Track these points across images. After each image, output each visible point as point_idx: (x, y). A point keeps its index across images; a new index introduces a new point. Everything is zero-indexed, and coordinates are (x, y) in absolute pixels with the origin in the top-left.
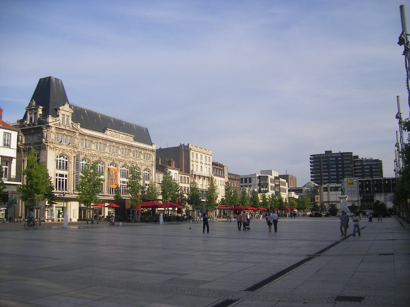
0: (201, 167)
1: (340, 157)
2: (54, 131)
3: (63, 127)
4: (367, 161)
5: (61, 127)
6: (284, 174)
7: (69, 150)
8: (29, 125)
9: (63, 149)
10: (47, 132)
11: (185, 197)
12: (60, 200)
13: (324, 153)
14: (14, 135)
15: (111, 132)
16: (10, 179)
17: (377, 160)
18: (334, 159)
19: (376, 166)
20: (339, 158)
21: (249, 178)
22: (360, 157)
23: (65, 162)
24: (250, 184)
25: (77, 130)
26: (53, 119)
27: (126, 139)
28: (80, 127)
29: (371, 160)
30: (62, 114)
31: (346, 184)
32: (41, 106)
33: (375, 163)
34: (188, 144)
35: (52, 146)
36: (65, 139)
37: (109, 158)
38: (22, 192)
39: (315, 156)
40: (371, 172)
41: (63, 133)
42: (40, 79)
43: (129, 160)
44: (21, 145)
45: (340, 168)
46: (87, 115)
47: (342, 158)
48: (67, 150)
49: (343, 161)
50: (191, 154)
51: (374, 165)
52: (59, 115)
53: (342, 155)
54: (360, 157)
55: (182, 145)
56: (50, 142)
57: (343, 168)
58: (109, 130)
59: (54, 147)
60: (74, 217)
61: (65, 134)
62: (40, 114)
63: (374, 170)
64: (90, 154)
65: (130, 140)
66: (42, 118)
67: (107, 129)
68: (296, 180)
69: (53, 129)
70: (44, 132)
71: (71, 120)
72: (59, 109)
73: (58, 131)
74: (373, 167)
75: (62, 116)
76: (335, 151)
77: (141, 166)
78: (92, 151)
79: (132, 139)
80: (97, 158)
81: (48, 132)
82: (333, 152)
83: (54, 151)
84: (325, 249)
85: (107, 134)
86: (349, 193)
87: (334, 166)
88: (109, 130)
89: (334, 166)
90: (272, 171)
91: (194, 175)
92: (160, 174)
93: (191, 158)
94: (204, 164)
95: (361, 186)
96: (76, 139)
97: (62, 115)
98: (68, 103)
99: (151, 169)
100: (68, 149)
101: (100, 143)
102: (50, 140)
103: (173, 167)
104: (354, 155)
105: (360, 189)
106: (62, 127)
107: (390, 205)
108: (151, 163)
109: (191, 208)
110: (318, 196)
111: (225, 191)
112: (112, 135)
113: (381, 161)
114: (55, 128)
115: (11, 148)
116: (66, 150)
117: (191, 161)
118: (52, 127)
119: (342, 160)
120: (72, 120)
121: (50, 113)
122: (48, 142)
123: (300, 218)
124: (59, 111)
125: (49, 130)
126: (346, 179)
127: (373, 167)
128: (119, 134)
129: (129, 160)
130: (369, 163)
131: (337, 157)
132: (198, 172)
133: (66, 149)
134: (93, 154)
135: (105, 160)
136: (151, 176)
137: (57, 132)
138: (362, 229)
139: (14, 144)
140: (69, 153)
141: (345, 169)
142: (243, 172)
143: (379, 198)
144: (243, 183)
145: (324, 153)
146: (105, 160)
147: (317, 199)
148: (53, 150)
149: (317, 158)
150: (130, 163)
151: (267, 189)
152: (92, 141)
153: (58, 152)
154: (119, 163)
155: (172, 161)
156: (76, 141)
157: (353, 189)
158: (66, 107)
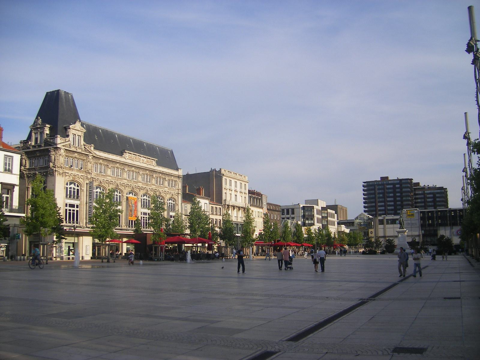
0: (236, 196)
1: (398, 184)
2: (64, 154)
3: (74, 150)
4: (429, 188)
5: (72, 149)
6: (333, 204)
7: (81, 175)
8: (34, 147)
9: (74, 175)
10: (55, 155)
11: (217, 231)
12: (70, 235)
13: (380, 180)
14: (17, 158)
15: (130, 155)
16: (12, 210)
17: (442, 188)
18: (392, 186)
19: (440, 194)
20: (397, 186)
21: (292, 209)
22: (422, 185)
23: (76, 190)
24: (293, 216)
25: (91, 153)
26: (62, 139)
27: (148, 164)
28: (94, 149)
29: (435, 188)
30: (73, 134)
31: (405, 216)
32: (49, 124)
33: (439, 191)
34: (221, 169)
35: (61, 172)
36: (76, 163)
37: (127, 186)
38: (25, 225)
39: (369, 183)
40: (434, 201)
41: (74, 156)
42: (47, 93)
43: (151, 188)
44: (24, 170)
45: (398, 197)
46: (102, 135)
47: (401, 185)
48: (78, 176)
49: (401, 189)
50: (223, 181)
51: (438, 193)
52: (69, 135)
53: (401, 182)
54: (422, 185)
55: (213, 170)
56: (59, 166)
57: (401, 197)
58: (127, 153)
59: (63, 172)
60: (86, 255)
61: (76, 157)
62: (47, 134)
63: (438, 199)
64: (105, 180)
65: (152, 164)
66: (49, 139)
67: (126, 151)
68: (346, 210)
69: (62, 151)
70: (52, 155)
71: (83, 141)
72: (70, 128)
73: (68, 154)
74: (437, 195)
75: (73, 136)
76: (392, 177)
77: (165, 194)
78: (108, 177)
79: (154, 163)
80: (114, 185)
81: (56, 155)
82: (390, 179)
83: (64, 178)
84: (380, 292)
85: (126, 157)
86: (408, 226)
87: (391, 195)
88: (127, 153)
89: (391, 195)
90: (319, 200)
91: (227, 205)
92: (188, 204)
93: (224, 186)
94: (239, 192)
95: (422, 218)
96: (89, 162)
97: (73, 135)
98: (80, 121)
99: (177, 198)
100: (80, 174)
101: (117, 168)
102: (58, 164)
103: (202, 195)
104: (414, 181)
105: (422, 221)
106: (73, 149)
107: (456, 240)
108: (177, 191)
109: (223, 244)
110: (373, 230)
111: (264, 224)
112: (131, 159)
113: (446, 189)
114: (64, 150)
115: (13, 173)
116: (77, 175)
117: (224, 189)
118: (61, 149)
119: (401, 188)
120: (84, 141)
121: (58, 133)
122: (56, 167)
123: (351, 256)
124: (69, 130)
125: (57, 152)
126: (405, 210)
127: (437, 195)
128: (140, 157)
129: (151, 188)
130: (432, 191)
131: (394, 185)
132: (232, 202)
133: (77, 175)
134: (109, 181)
135: (123, 187)
136: (177, 206)
137: (67, 155)
138: (424, 268)
139: (16, 169)
140: (80, 179)
141: (404, 198)
142: (285, 202)
143: (444, 232)
144: (284, 215)
145: (380, 180)
146: (123, 187)
147: (371, 234)
148: (62, 175)
149: (371, 185)
150: (152, 191)
151: (312, 222)
152: (107, 165)
153: (68, 178)
154: (140, 191)
155: (201, 188)
156: (89, 165)
157: (413, 222)
158: (78, 125)
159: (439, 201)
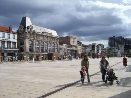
6: (100, 44)
11: (102, 46)
13: (63, 44)
14: (16, 36)
16: (16, 49)
19: (82, 61)
31: (120, 47)
38: (15, 57)
40: (128, 43)
53: (119, 37)
57: (119, 43)
69: (28, 33)
82: (52, 35)
84: (66, 88)
93: (70, 40)
104: (122, 37)
106: (30, 32)
109: (70, 56)
111: (8, 52)
123: (7, 41)
126: (120, 45)
138: (90, 68)
139: (16, 38)
145: (63, 44)
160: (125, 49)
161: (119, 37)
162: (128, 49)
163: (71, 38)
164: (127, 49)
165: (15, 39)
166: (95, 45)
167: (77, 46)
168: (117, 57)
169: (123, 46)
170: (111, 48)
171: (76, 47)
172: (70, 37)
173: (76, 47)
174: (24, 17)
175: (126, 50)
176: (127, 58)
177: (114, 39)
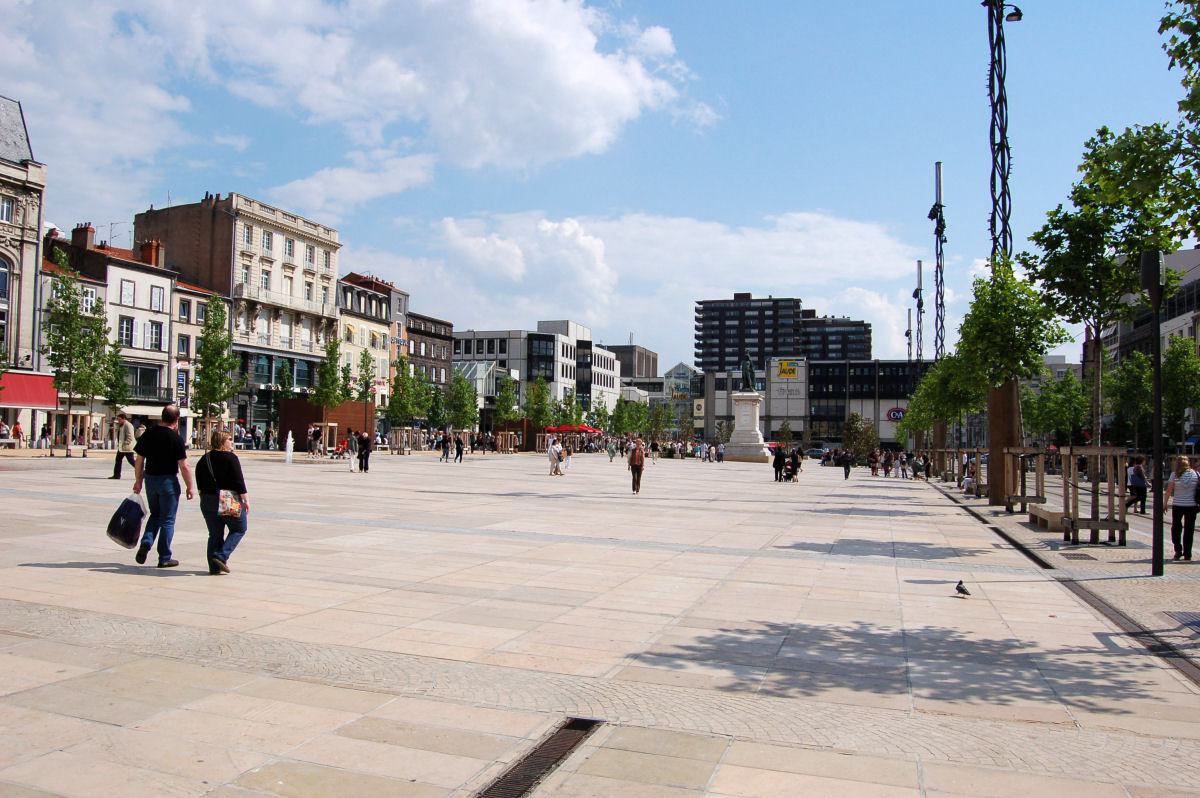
1: (768, 308)
4: (835, 323)
17: (861, 324)
18: (756, 313)
20: (768, 313)
22: (819, 315)
24: (503, 356)
29: (846, 323)
31: (774, 371)
33: (854, 329)
39: (708, 305)
45: (769, 336)
47: (775, 312)
49: (776, 321)
50: (237, 233)
51: (853, 333)
53: (776, 304)
54: (819, 315)
55: (211, 196)
68: (655, 360)
74: (852, 337)
82: (753, 297)
87: (755, 331)
89: (755, 331)
90: (570, 324)
91: (328, 319)
94: (256, 259)
95: (811, 380)
103: (157, 264)
104: (804, 306)
105: (812, 387)
107: (888, 431)
108: (18, 232)
110: (702, 402)
113: (870, 325)
117: (238, 253)
127: (852, 337)
131: (762, 309)
136: (16, 283)
140: (10, 248)
141: (781, 340)
142: (470, 317)
143: (862, 410)
144: (482, 353)
147: (699, 405)
149: (713, 310)
157: (791, 386)
159: (854, 342)
160: (811, 396)
161: (776, 301)
162: (839, 395)
163: (252, 221)
164: (828, 396)
165: (188, 322)
166: (561, 339)
167: (331, 322)
168: (230, 550)
169: (801, 373)
170: (702, 379)
171: (323, 325)
172: (238, 213)
173: (323, 325)
174: (564, 322)
175: (823, 403)
176: (1192, 233)
177: (742, 318)
